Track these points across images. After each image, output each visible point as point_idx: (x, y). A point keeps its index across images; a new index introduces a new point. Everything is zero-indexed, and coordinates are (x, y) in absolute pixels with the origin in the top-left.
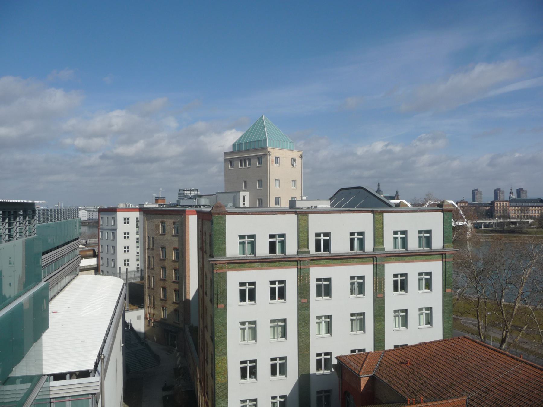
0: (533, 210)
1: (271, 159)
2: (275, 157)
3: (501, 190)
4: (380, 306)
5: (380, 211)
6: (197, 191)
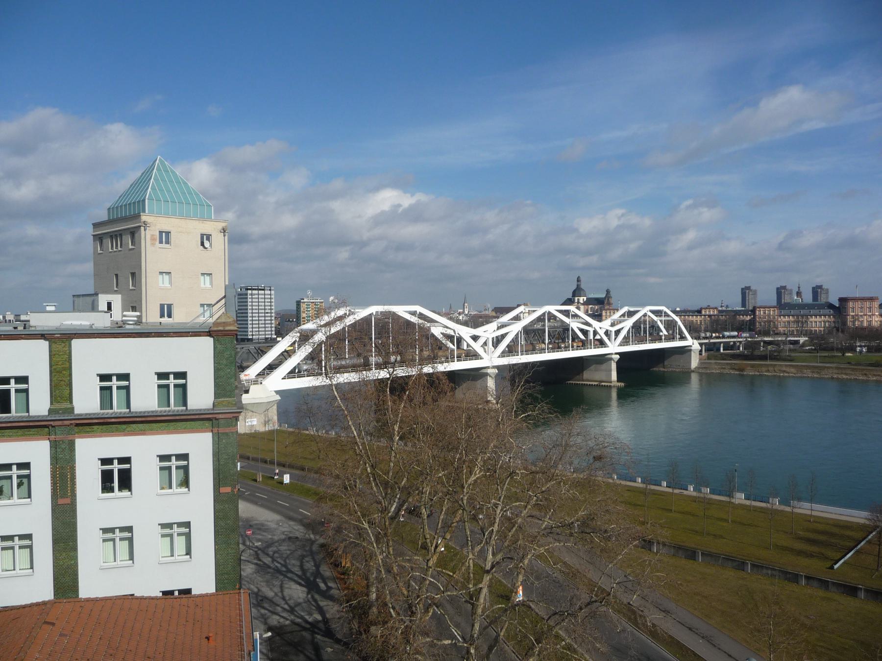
0: (816, 322)
1: (147, 236)
2: (161, 233)
3: (787, 288)
5: (59, 335)
6: (270, 290)
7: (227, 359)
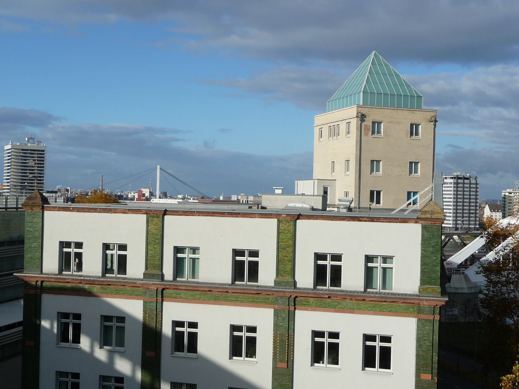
7: (433, 247)
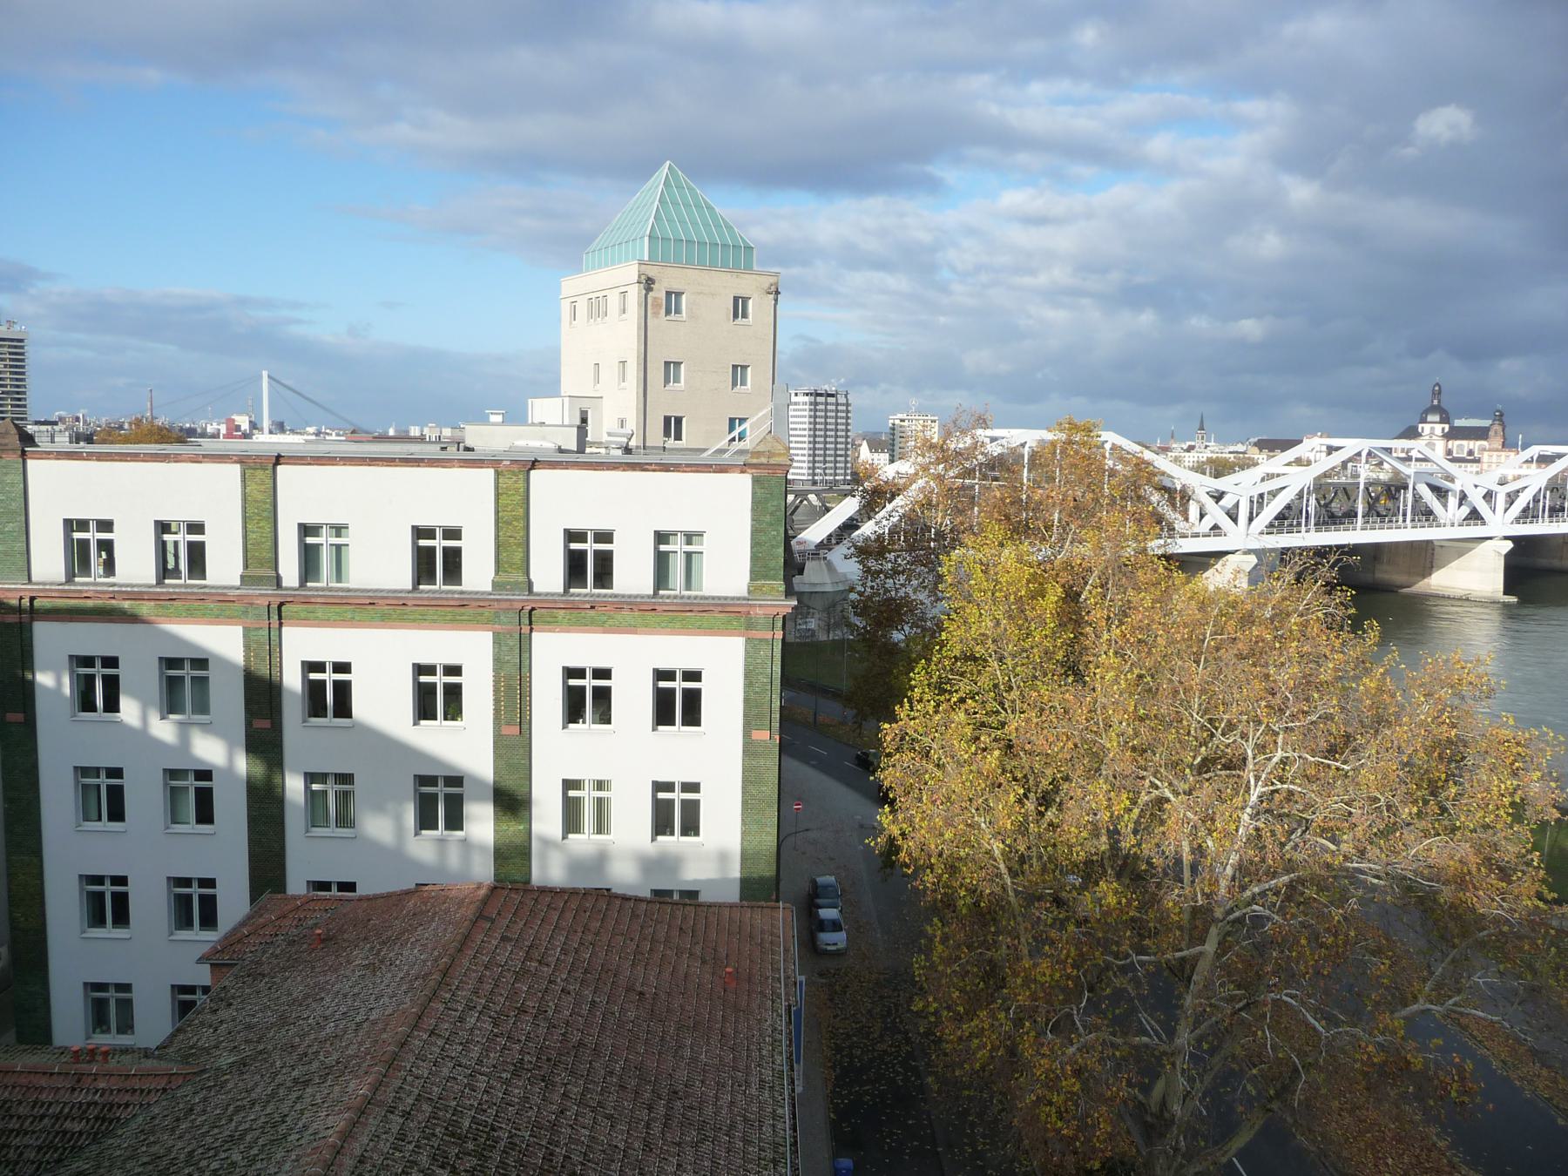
4: (511, 761)
